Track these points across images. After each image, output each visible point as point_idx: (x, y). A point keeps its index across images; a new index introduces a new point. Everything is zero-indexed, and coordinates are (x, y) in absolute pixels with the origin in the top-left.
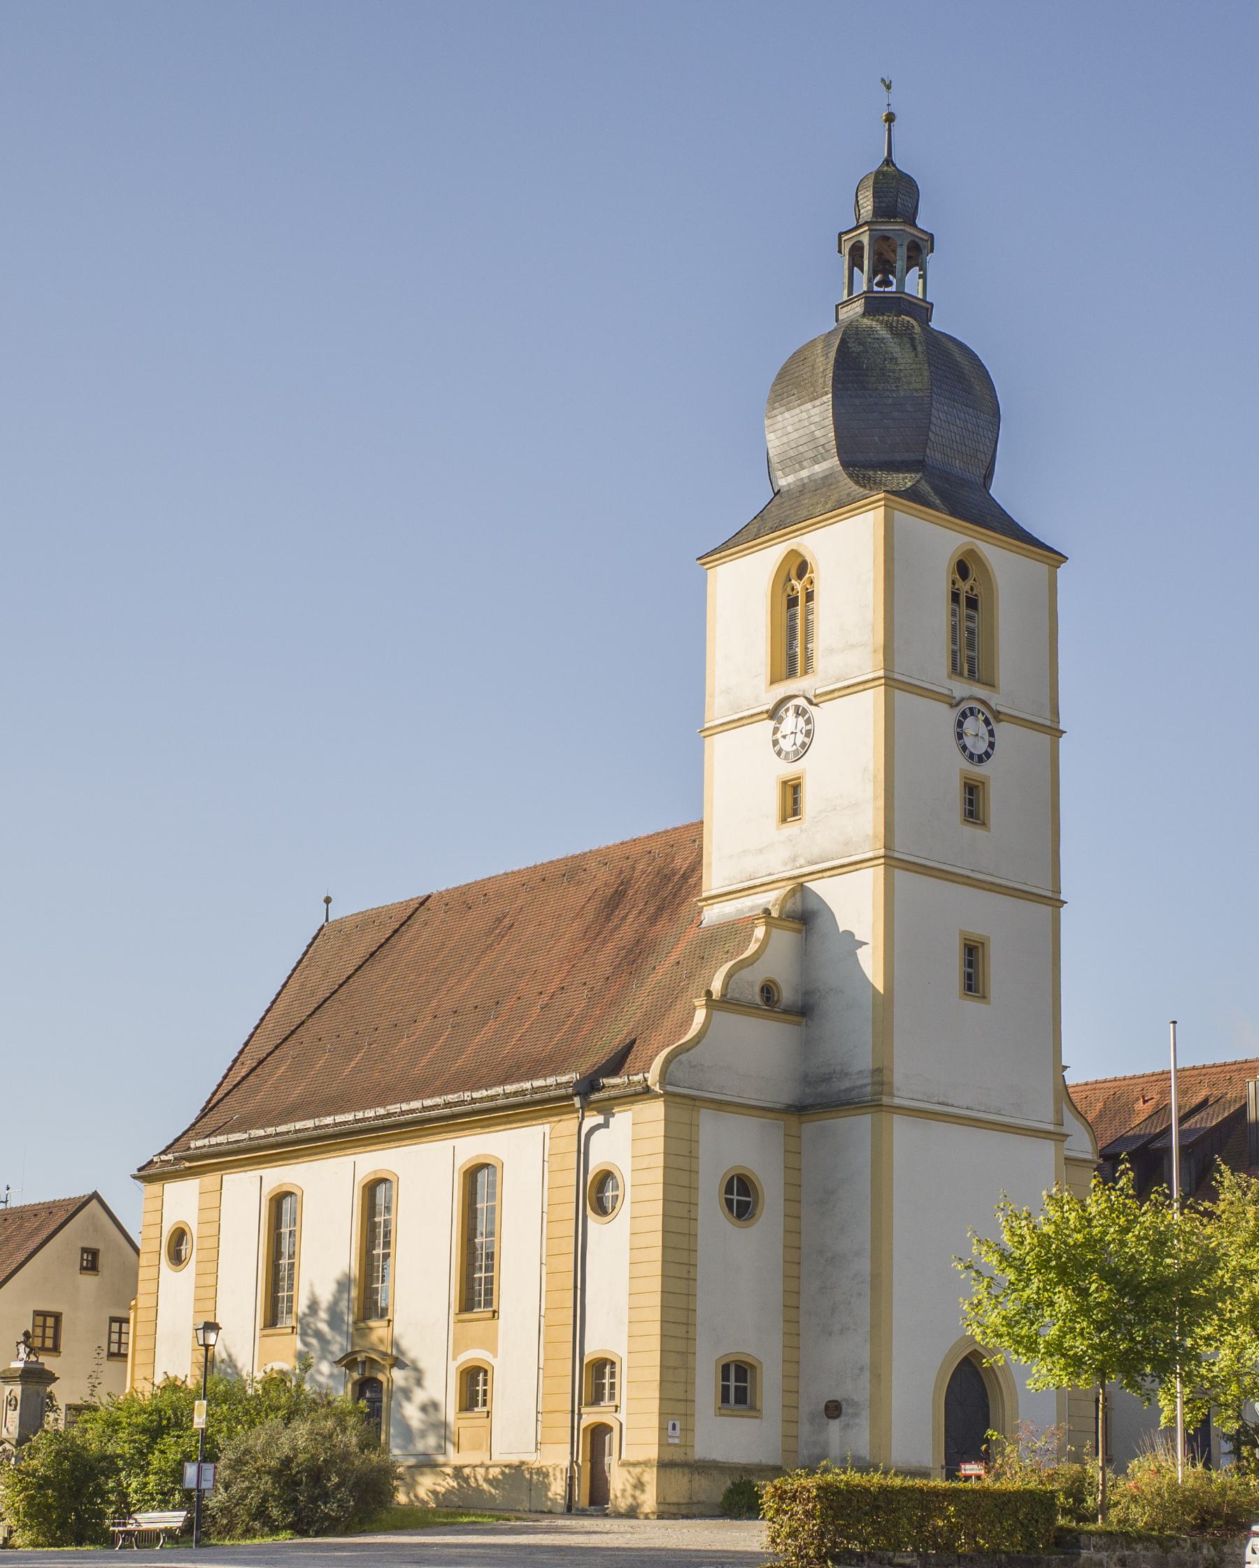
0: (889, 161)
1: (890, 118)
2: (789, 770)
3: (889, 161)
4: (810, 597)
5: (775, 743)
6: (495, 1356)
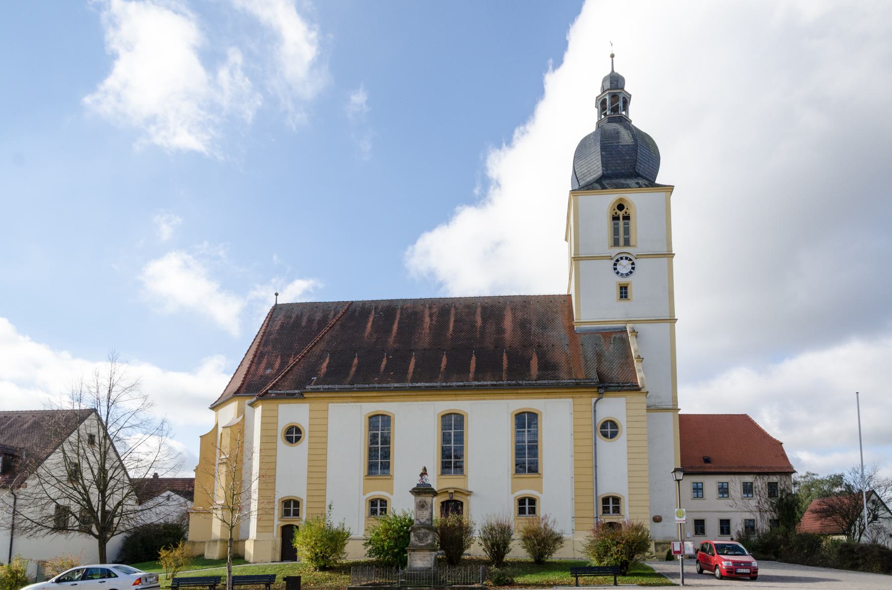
0: (613, 71)
1: (612, 56)
2: (624, 281)
3: (613, 71)
4: (627, 218)
5: (631, 272)
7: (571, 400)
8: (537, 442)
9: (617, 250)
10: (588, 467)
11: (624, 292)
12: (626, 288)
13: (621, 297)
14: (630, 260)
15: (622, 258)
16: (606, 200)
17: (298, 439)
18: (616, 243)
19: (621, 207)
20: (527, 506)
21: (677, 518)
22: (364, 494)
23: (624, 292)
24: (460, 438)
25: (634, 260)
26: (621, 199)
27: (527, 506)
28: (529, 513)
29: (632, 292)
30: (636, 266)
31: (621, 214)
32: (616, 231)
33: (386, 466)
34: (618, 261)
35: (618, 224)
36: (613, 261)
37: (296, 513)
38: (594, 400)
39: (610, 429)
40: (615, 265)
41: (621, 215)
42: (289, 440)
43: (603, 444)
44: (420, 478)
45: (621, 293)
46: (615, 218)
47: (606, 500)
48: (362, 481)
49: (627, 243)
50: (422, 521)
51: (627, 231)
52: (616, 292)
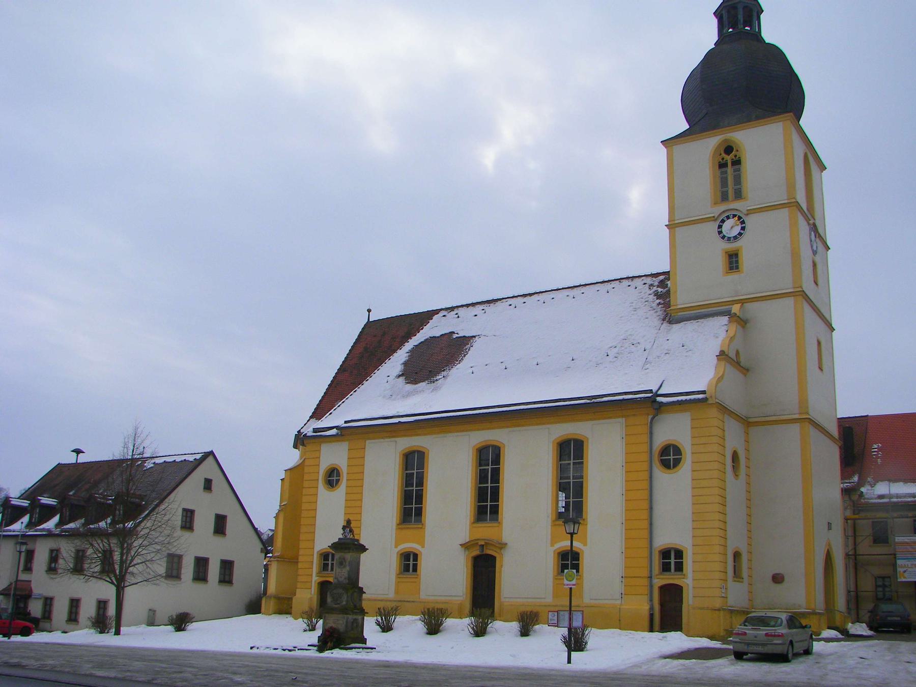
2: (731, 246)
4: (737, 162)
6: (423, 547)
7: (622, 420)
8: (582, 477)
9: (723, 207)
10: (643, 508)
11: (733, 261)
12: (736, 255)
13: (731, 269)
14: (734, 216)
15: (728, 218)
16: (710, 144)
17: (677, 462)
18: (724, 198)
19: (729, 150)
20: (673, 561)
21: (566, 582)
22: (396, 547)
23: (733, 261)
24: (496, 474)
25: (744, 218)
26: (726, 141)
27: (673, 561)
28: (676, 570)
29: (745, 260)
30: (748, 225)
31: (729, 158)
32: (724, 182)
33: (495, 510)
34: (723, 221)
35: (726, 172)
36: (718, 223)
37: (679, 567)
38: (650, 417)
39: (670, 457)
40: (720, 227)
41: (729, 161)
42: (666, 465)
43: (662, 477)
44: (342, 532)
45: (731, 263)
46: (722, 165)
47: (665, 554)
48: (394, 531)
49: (739, 195)
50: (341, 579)
51: (738, 179)
52: (720, 262)
